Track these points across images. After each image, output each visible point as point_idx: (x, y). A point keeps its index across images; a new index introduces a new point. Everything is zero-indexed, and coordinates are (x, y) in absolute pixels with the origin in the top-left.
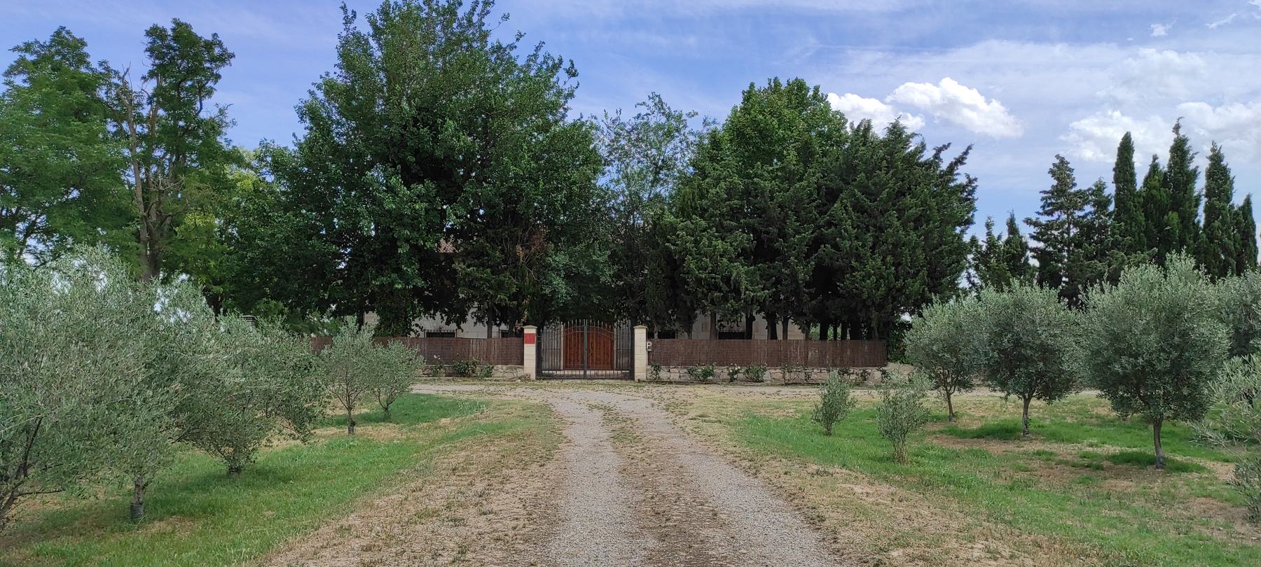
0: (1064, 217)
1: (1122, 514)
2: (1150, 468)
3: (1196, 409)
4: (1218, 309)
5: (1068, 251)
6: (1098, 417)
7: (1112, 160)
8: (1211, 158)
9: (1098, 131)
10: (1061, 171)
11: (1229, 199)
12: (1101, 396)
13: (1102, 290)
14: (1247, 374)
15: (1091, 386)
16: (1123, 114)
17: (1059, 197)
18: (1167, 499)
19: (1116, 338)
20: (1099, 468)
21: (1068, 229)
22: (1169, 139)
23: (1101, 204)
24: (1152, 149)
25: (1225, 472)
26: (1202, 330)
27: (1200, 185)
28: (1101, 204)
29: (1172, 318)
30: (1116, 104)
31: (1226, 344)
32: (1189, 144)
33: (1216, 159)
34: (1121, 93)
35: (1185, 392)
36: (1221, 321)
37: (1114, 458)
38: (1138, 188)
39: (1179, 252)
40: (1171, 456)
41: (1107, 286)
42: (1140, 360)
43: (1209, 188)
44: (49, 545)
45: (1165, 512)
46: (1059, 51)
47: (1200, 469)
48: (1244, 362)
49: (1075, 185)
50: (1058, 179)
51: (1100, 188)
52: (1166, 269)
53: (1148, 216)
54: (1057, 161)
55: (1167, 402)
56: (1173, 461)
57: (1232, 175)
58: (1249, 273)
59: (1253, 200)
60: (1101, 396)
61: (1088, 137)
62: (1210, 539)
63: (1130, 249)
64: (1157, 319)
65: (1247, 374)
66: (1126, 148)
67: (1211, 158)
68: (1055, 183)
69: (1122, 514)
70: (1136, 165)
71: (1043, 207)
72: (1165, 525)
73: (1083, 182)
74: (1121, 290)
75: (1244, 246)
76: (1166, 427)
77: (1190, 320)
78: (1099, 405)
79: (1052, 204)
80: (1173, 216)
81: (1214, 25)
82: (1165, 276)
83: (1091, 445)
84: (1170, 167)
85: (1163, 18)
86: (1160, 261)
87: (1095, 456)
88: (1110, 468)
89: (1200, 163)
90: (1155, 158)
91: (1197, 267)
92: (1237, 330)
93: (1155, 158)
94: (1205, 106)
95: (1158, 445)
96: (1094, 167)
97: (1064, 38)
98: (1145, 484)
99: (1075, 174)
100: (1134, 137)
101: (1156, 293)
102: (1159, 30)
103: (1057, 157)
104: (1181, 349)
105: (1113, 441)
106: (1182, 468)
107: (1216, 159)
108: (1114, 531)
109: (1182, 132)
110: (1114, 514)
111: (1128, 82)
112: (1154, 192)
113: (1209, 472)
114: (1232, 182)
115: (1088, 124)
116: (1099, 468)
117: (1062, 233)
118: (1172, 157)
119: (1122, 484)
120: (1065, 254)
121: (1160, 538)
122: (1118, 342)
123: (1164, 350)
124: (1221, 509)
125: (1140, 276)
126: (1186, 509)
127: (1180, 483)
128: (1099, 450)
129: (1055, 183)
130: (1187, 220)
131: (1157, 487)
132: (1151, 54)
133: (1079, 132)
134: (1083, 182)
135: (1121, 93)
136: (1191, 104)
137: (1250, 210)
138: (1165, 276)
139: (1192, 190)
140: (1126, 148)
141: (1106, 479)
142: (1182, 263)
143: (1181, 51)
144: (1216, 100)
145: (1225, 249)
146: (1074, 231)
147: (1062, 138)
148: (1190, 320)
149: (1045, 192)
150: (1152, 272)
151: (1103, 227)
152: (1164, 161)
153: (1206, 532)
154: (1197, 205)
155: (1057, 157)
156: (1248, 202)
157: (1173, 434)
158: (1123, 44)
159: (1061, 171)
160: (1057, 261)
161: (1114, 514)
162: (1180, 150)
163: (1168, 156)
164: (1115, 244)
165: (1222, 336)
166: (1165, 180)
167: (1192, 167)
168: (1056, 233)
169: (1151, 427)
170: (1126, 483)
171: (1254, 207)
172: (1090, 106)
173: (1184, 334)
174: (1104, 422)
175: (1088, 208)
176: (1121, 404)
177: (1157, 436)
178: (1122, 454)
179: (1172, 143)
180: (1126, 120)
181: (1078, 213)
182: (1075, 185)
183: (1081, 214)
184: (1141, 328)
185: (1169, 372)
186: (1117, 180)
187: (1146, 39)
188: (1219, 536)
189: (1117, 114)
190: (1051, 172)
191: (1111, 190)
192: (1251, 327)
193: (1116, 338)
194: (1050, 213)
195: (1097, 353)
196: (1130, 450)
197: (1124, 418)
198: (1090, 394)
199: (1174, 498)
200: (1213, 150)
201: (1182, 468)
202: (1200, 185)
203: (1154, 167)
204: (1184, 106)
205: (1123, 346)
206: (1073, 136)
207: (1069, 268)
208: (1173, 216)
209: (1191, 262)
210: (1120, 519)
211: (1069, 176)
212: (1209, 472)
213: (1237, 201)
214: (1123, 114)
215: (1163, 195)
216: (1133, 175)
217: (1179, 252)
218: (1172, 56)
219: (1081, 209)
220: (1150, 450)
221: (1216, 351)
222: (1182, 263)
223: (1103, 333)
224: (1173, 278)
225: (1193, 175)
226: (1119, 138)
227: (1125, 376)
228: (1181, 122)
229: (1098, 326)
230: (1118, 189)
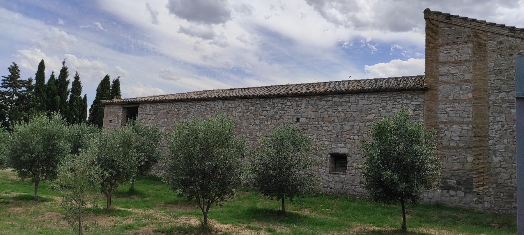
0: (12, 90)
1: (14, 223)
2: (31, 201)
3: (53, 175)
4: (69, 136)
5: (11, 106)
6: (12, 180)
7: (36, 70)
8: (75, 78)
9: (30, 56)
10: (14, 69)
11: (80, 94)
12: (14, 171)
13: (21, 124)
14: (72, 161)
15: (12, 167)
16: (42, 52)
17: (10, 81)
18: (36, 214)
19: (24, 145)
20: (8, 203)
21: (13, 96)
22: (61, 67)
23: (30, 88)
24: (53, 69)
25: (59, 200)
26: (61, 144)
27: (70, 87)
28: (30, 88)
29: (50, 138)
30: (39, 46)
31: (69, 150)
32: (68, 70)
33: (77, 78)
34: (43, 43)
35: (51, 169)
36: (69, 141)
37: (16, 198)
38: (45, 83)
39: (57, 112)
40: (41, 196)
41: (22, 122)
42: (34, 155)
43: (72, 89)
44: (454, 214)
45: (34, 220)
46: (17, 16)
47: (52, 200)
48: (72, 157)
49: (19, 77)
50: (12, 73)
51: (30, 81)
52: (50, 118)
53: (48, 96)
54: (13, 65)
55: (43, 173)
56: (41, 198)
57: (82, 86)
58: (82, 123)
59: (87, 96)
60: (14, 171)
61: (25, 58)
62: (50, 228)
63: (40, 109)
64: (43, 138)
65: (72, 161)
66: (42, 66)
67: (75, 78)
68: (10, 74)
69: (14, 223)
70: (45, 74)
71: (2, 84)
72: (32, 225)
73: (23, 76)
74: (30, 125)
75: (83, 113)
76: (41, 183)
77: (56, 140)
78: (14, 175)
79: (7, 83)
80: (58, 98)
81: (82, 27)
82: (50, 121)
83: (6, 193)
84: (59, 77)
85: (64, 18)
86: (49, 115)
87: (8, 198)
88: (13, 203)
89: (71, 78)
90: (53, 73)
91: (63, 119)
92: (74, 145)
93: (53, 73)
94: (74, 56)
95: (36, 192)
96: (28, 72)
97: (20, 12)
98: (28, 208)
99: (20, 73)
100: (45, 62)
101: (45, 127)
102: (61, 22)
103: (13, 63)
104: (51, 151)
105: (18, 190)
106: (45, 200)
107: (77, 78)
108: (8, 231)
109: (65, 65)
110: (10, 223)
111: (46, 39)
112: (51, 86)
113: (55, 201)
114: (81, 88)
115: (26, 52)
116: (8, 203)
117: (9, 98)
118: (61, 74)
119: (17, 209)
120: (10, 107)
121: (29, 231)
122: (25, 147)
123: (44, 151)
124: (57, 216)
125: (39, 120)
126: (43, 217)
127: (42, 207)
128: (9, 195)
129: (10, 74)
130: (64, 99)
131: (32, 209)
132: (56, 31)
133: (22, 54)
134: (23, 76)
135: (43, 43)
136: (70, 55)
137: (86, 100)
138: (50, 121)
139: (67, 88)
140: (42, 66)
141: (10, 207)
142: (57, 116)
143: (68, 33)
144: (79, 56)
145: (76, 114)
146: (15, 97)
147: (13, 55)
148: (56, 140)
149: (4, 77)
150: (45, 119)
151: (29, 97)
152: (57, 75)
153: (49, 226)
154: (68, 95)
155: (13, 63)
156: (85, 97)
157: (44, 187)
158: (47, 23)
159: (14, 69)
160: (5, 110)
161: (10, 223)
162: (64, 72)
163: (59, 73)
164: (33, 106)
165: (68, 146)
166: (56, 82)
167: (67, 79)
168: (7, 97)
169: (34, 184)
170: (19, 209)
171: (87, 99)
172: (29, 45)
173: (54, 145)
174: (14, 182)
175: (24, 89)
176: (22, 174)
177: (36, 187)
178: (20, 196)
179: (61, 69)
180: (43, 54)
181: (19, 90)
182: (19, 77)
183: (20, 90)
184: (36, 141)
185: (45, 160)
186: (37, 79)
187: (55, 24)
188: (53, 227)
189: (39, 51)
190: (9, 69)
191: (34, 82)
192: (80, 144)
193: (24, 145)
194: (6, 87)
195: (15, 152)
196: (23, 194)
197: (23, 180)
198: (9, 170)
199: (39, 213)
200: (76, 75)
201: (45, 200)
202: (70, 87)
203: (52, 76)
204: (66, 54)
205: (27, 149)
206: (19, 55)
207: (10, 113)
208: (58, 98)
209: (61, 117)
210: (12, 225)
211: (17, 73)
212: (55, 201)
213: (82, 96)
214: (42, 52)
215: (55, 88)
216: (44, 78)
217: (57, 112)
218: (64, 33)
219: (21, 89)
220: (32, 194)
221: (65, 153)
222: (57, 116)
223: (19, 143)
224: (53, 122)
225: (68, 82)
226: (40, 61)
227: (26, 162)
228: (66, 62)
229: (17, 140)
230: (37, 82)
